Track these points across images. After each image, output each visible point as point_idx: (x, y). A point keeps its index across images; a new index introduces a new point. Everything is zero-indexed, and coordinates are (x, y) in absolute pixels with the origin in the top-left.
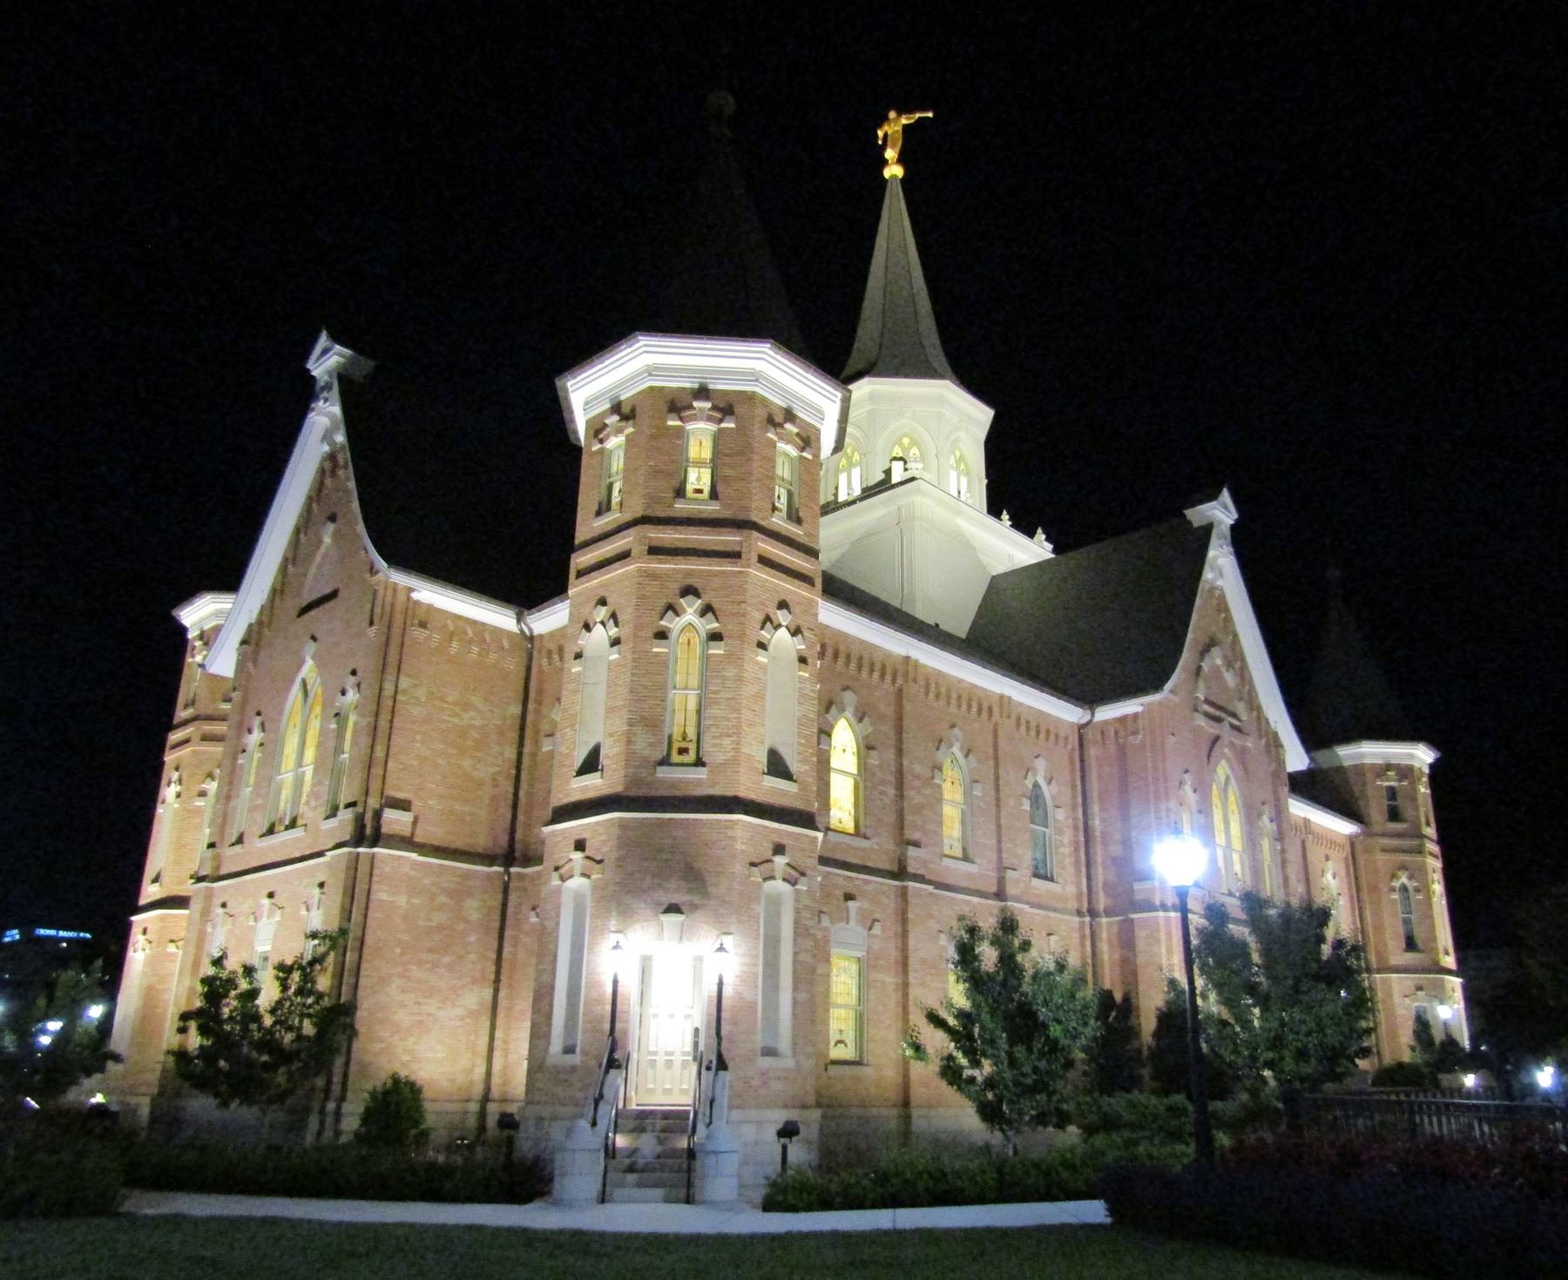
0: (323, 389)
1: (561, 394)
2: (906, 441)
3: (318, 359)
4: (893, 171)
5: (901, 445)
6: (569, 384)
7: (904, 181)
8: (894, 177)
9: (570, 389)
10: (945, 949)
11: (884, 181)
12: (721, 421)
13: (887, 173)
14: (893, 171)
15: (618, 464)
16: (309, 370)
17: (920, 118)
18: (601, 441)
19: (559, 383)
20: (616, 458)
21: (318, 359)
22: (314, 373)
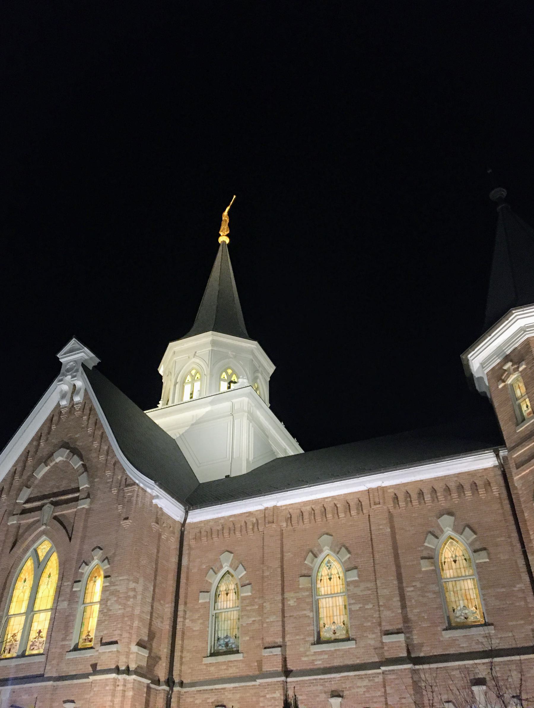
0: (68, 371)
1: (464, 363)
2: (230, 371)
3: (65, 354)
4: (224, 239)
5: (227, 373)
6: (469, 356)
7: (229, 245)
8: (224, 242)
9: (470, 359)
10: (89, 668)
11: (219, 244)
12: (518, 368)
13: (221, 240)
14: (224, 239)
15: (520, 391)
16: (58, 359)
17: (229, 213)
18: (504, 381)
19: (463, 357)
20: (90, 392)
21: (65, 354)
22: (61, 360)
